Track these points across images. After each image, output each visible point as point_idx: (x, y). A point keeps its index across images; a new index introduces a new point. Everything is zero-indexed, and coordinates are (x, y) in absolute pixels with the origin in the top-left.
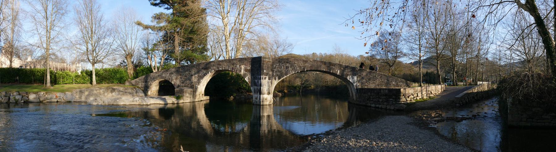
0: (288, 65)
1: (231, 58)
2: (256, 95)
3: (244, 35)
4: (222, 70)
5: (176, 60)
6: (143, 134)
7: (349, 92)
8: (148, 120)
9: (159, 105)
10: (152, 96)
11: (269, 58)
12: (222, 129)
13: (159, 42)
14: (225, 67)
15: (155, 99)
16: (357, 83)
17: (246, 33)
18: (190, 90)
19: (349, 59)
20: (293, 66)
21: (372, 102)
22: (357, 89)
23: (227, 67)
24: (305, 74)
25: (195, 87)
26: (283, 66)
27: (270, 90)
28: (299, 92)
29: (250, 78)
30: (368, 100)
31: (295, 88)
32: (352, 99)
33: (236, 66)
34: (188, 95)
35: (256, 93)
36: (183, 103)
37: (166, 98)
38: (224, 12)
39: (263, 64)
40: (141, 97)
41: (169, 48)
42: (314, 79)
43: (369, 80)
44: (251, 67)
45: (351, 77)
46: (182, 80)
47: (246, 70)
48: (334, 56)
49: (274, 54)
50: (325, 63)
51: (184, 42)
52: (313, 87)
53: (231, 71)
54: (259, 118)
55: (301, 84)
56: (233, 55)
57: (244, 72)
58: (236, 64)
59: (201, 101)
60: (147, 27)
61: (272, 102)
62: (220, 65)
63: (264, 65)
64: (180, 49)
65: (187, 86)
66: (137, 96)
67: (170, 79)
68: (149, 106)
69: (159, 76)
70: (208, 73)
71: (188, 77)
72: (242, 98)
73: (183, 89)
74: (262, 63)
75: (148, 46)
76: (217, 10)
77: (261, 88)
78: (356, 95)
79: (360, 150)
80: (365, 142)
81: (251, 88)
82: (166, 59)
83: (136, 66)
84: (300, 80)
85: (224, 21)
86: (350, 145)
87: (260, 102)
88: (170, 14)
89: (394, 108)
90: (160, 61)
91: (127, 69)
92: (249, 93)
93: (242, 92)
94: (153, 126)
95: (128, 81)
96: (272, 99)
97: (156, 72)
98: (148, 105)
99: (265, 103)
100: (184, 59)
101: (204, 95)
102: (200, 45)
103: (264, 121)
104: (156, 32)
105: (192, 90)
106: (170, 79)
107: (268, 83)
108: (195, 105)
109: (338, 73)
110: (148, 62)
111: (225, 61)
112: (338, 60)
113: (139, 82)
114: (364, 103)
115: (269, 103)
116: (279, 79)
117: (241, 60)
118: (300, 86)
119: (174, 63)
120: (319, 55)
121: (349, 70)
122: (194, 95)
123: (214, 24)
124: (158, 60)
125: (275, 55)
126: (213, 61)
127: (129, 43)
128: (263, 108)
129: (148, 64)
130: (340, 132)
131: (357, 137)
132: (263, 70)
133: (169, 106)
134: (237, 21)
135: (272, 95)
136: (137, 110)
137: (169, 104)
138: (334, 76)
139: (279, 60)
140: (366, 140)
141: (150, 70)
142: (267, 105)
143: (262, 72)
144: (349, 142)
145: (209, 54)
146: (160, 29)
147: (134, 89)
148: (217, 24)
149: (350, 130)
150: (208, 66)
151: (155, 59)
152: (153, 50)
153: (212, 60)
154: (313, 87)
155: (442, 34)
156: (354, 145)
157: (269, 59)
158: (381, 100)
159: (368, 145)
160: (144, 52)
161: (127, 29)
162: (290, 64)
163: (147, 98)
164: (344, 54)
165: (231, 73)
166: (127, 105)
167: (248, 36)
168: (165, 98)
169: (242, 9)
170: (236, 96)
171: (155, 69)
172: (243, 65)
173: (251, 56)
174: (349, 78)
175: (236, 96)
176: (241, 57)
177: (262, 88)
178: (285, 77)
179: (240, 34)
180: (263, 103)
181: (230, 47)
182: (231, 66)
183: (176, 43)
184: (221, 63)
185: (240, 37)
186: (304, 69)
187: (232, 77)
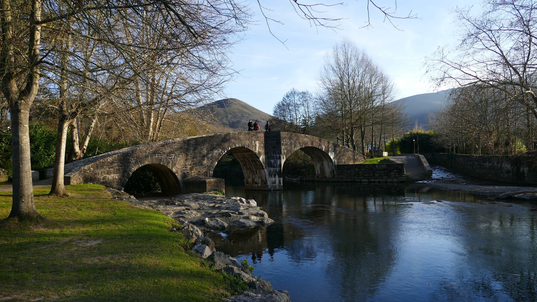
2: (273, 178)
35: (273, 176)
89: (398, 181)
155: (89, 51)
158: (376, 175)
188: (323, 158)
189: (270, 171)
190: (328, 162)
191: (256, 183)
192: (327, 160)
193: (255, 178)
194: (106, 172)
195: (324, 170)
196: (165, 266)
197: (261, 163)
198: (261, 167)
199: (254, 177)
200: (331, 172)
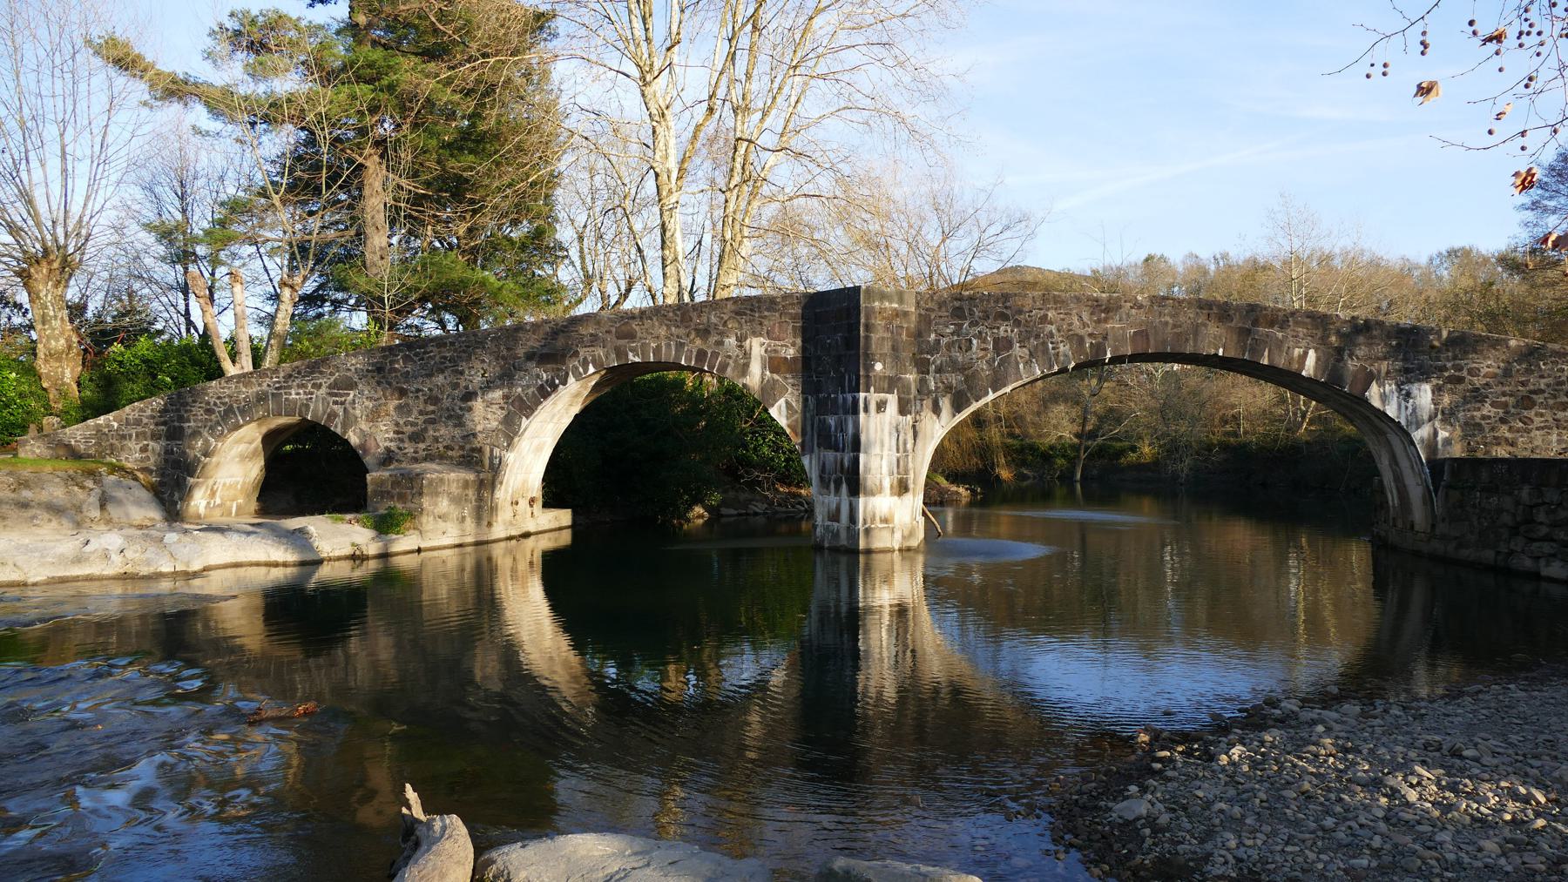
0: (1004, 330)
1: (692, 297)
3: (759, 169)
4: (644, 367)
5: (370, 302)
6: (151, 753)
7: (1381, 482)
8: (191, 664)
9: (263, 570)
10: (217, 518)
11: (901, 297)
12: (645, 682)
13: (263, 193)
14: (659, 348)
15: (235, 537)
16: (1437, 424)
17: (772, 159)
18: (455, 478)
19: (1374, 281)
20: (1037, 337)
21: (1547, 548)
22: (1437, 466)
23: (668, 346)
24: (1101, 379)
25: (492, 458)
26: (979, 336)
27: (906, 472)
28: (1067, 478)
29: (797, 405)
30: (1514, 531)
31: (1046, 457)
32: (1400, 524)
33: (720, 343)
34: (444, 505)
35: (832, 486)
36: (419, 550)
37: (312, 529)
38: (647, 39)
39: (868, 327)
40: (140, 527)
41: (331, 233)
42: (1152, 403)
43: (1526, 402)
44: (804, 349)
45: (1390, 387)
46: (413, 424)
47: (774, 363)
48: (1278, 265)
49: (926, 270)
50: (1222, 312)
51: (417, 200)
52: (1147, 450)
53: (693, 370)
54: (852, 620)
55: (1077, 435)
56: (702, 282)
57: (763, 374)
58: (722, 334)
59: (526, 535)
60: (176, 90)
61: (921, 535)
62: (631, 336)
63: (874, 337)
64: (395, 240)
65: (441, 458)
66: (109, 522)
67: (333, 415)
68: (197, 582)
69: (261, 398)
70: (564, 383)
71: (446, 403)
72: (756, 514)
73: (418, 475)
74: (862, 321)
75: (184, 211)
76: (608, 32)
77: (856, 461)
78: (1428, 500)
79: (1482, 843)
80: (1515, 796)
81: (806, 461)
82: (311, 300)
83: (104, 333)
84: (1074, 415)
85: (648, 90)
86: (1408, 804)
87: (854, 536)
88: (335, 26)
90: (270, 309)
91: (34, 349)
92: (794, 489)
93: (754, 484)
94: (229, 692)
95: (40, 429)
96: (922, 520)
97: (242, 378)
98: (189, 576)
99: (881, 540)
100: (423, 300)
101: (539, 503)
102: (515, 223)
103: (879, 639)
104: (237, 131)
105: (471, 477)
106: (333, 415)
107: (898, 431)
108: (490, 559)
109: (1310, 367)
110: (187, 314)
111: (657, 313)
112: (1299, 291)
113: (123, 437)
114: (1488, 555)
115: (904, 537)
116: (958, 407)
117: (751, 311)
118: (1075, 448)
119: (359, 320)
120: (1180, 269)
121: (1380, 349)
122: (483, 510)
123: (596, 108)
124: (253, 300)
125: (931, 276)
126: (587, 317)
127: (44, 180)
128: (868, 568)
129: (190, 323)
130: (1334, 715)
131: (1451, 761)
132: (870, 360)
133: (325, 573)
134: (721, 93)
135: (921, 497)
136: (112, 609)
137: (330, 559)
138: (1279, 383)
139: (957, 304)
140: (1522, 790)
141: (201, 364)
142: (891, 551)
143: (862, 373)
144: (1397, 780)
145: (566, 275)
146: (270, 114)
147: (89, 484)
148: (612, 110)
149: (1395, 711)
150: (560, 342)
151: (239, 298)
152: (220, 235)
153: (581, 310)
154: (1147, 450)
156: (1433, 804)
157: (901, 301)
159: (1540, 823)
160: (161, 250)
161: (33, 86)
162: (1017, 323)
163: (186, 531)
164: (1337, 251)
165: (690, 380)
166: (35, 584)
167: (782, 173)
168: (302, 531)
169: (749, 27)
170: (719, 506)
171: (234, 355)
172: (755, 334)
173: (802, 288)
174: (1382, 397)
175: (723, 503)
176: (747, 292)
177: (862, 457)
178: (991, 396)
179: (738, 166)
180: (868, 543)
181: (684, 236)
182: (692, 341)
183: (376, 200)
184: (637, 328)
185: (737, 179)
186: (1099, 348)
187: (695, 401)
188: (396, 436)
189: (824, 464)
194: (149, 433)
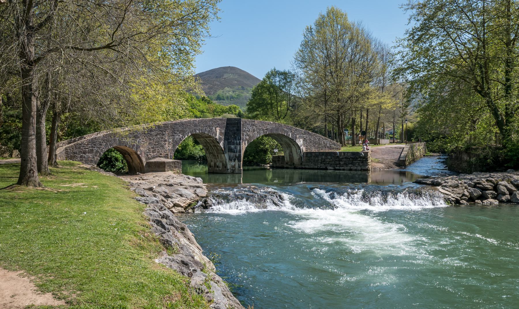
35: (233, 160)
190: (296, 149)
191: (218, 167)
192: (295, 147)
193: (217, 161)
195: (293, 157)
196: (14, 275)
197: (222, 148)
198: (222, 152)
199: (216, 160)
200: (299, 159)
